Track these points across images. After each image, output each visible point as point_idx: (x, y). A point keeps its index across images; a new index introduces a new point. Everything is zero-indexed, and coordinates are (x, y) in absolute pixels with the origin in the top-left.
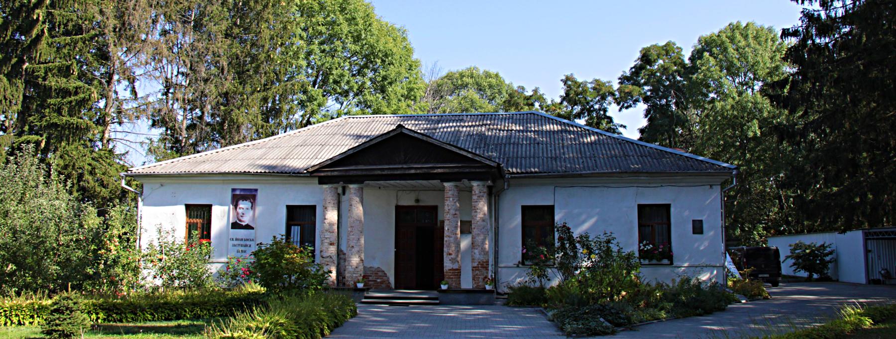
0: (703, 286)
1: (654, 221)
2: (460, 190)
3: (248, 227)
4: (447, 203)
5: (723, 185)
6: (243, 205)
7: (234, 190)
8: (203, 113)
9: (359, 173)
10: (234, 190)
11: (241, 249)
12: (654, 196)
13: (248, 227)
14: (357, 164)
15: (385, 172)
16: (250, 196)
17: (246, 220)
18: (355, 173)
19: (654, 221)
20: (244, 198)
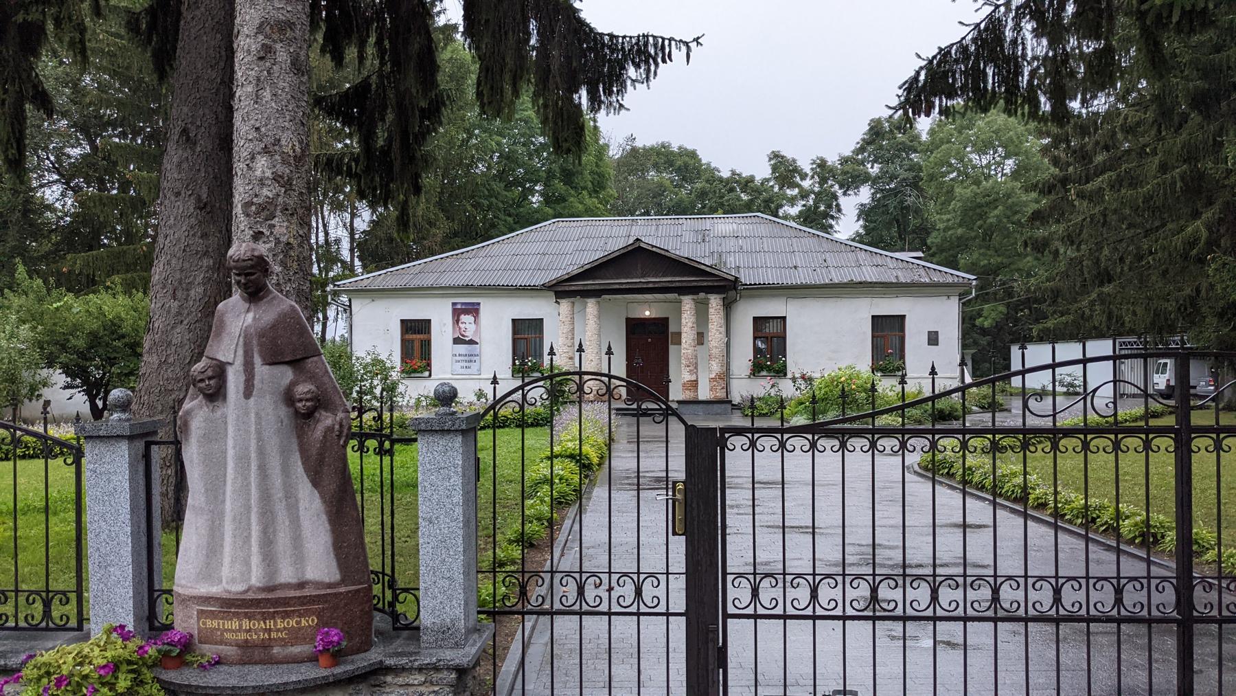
0: (31, 408)
1: (887, 333)
2: (696, 302)
3: (472, 342)
4: (684, 316)
5: (961, 296)
6: (467, 319)
7: (454, 304)
8: (157, 233)
9: (598, 287)
10: (454, 304)
11: (465, 364)
12: (415, 309)
13: (472, 342)
14: (594, 279)
15: (651, 286)
16: (473, 310)
17: (469, 335)
18: (593, 287)
19: (887, 333)
20: (466, 312)
